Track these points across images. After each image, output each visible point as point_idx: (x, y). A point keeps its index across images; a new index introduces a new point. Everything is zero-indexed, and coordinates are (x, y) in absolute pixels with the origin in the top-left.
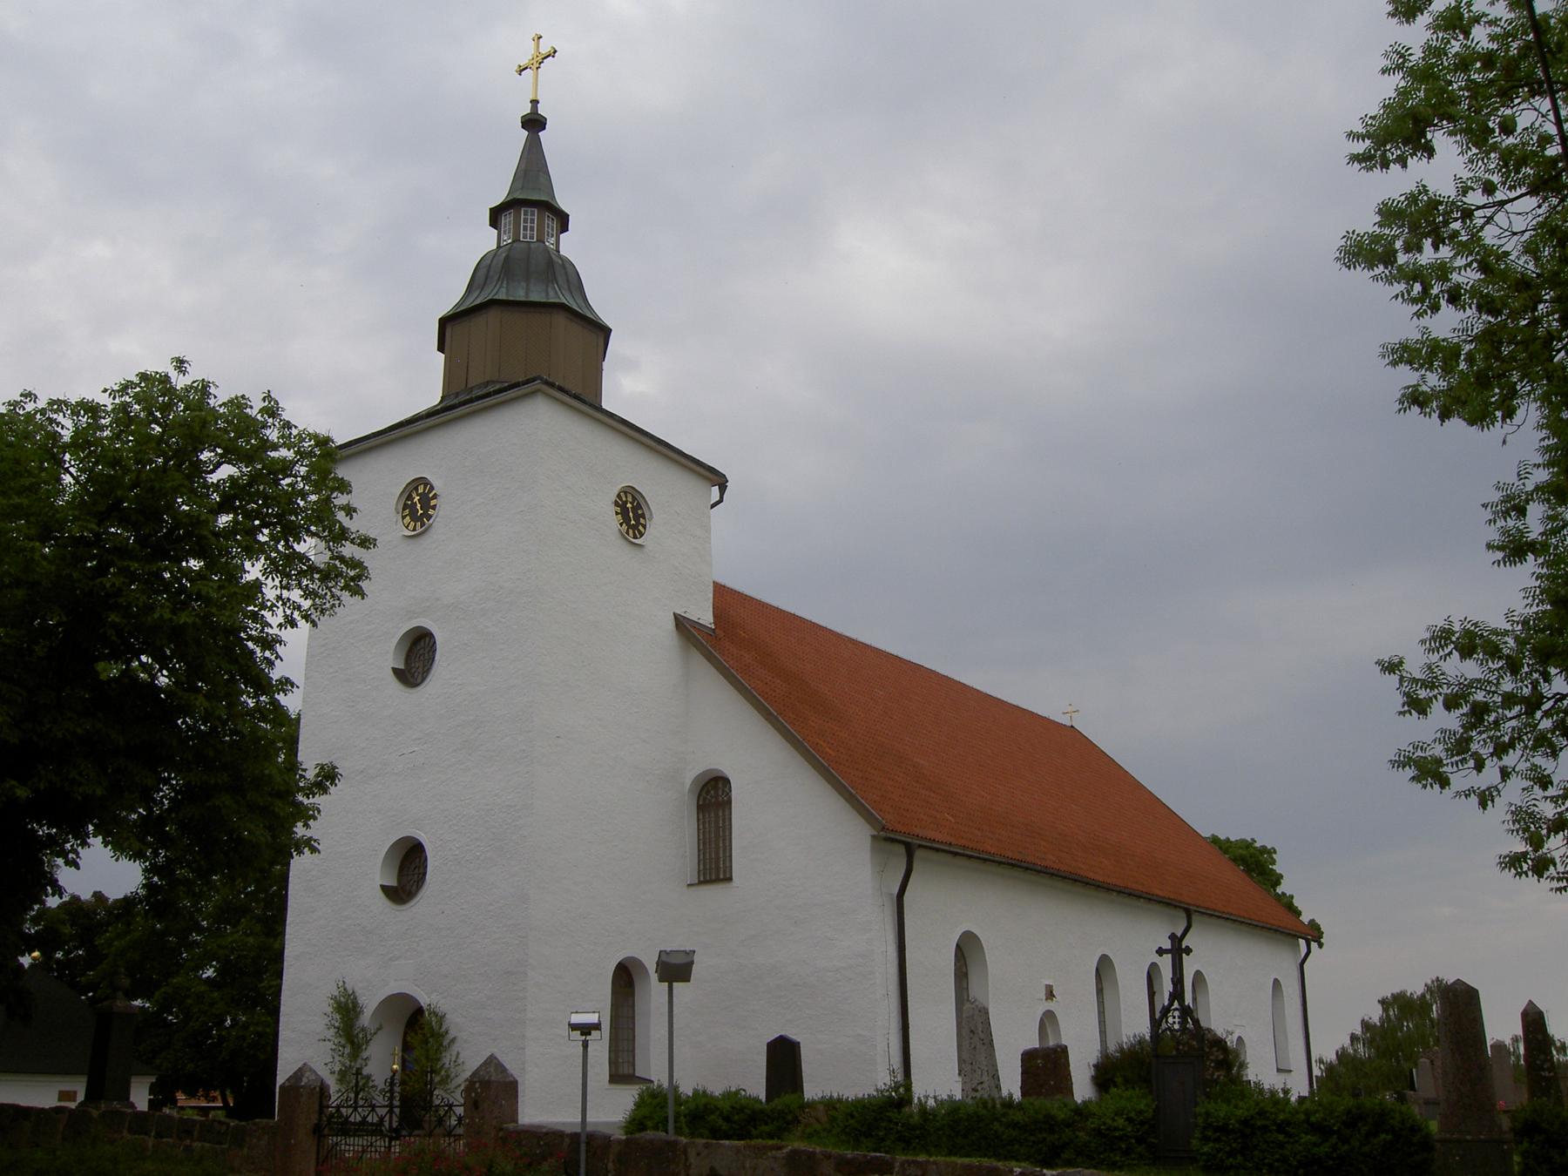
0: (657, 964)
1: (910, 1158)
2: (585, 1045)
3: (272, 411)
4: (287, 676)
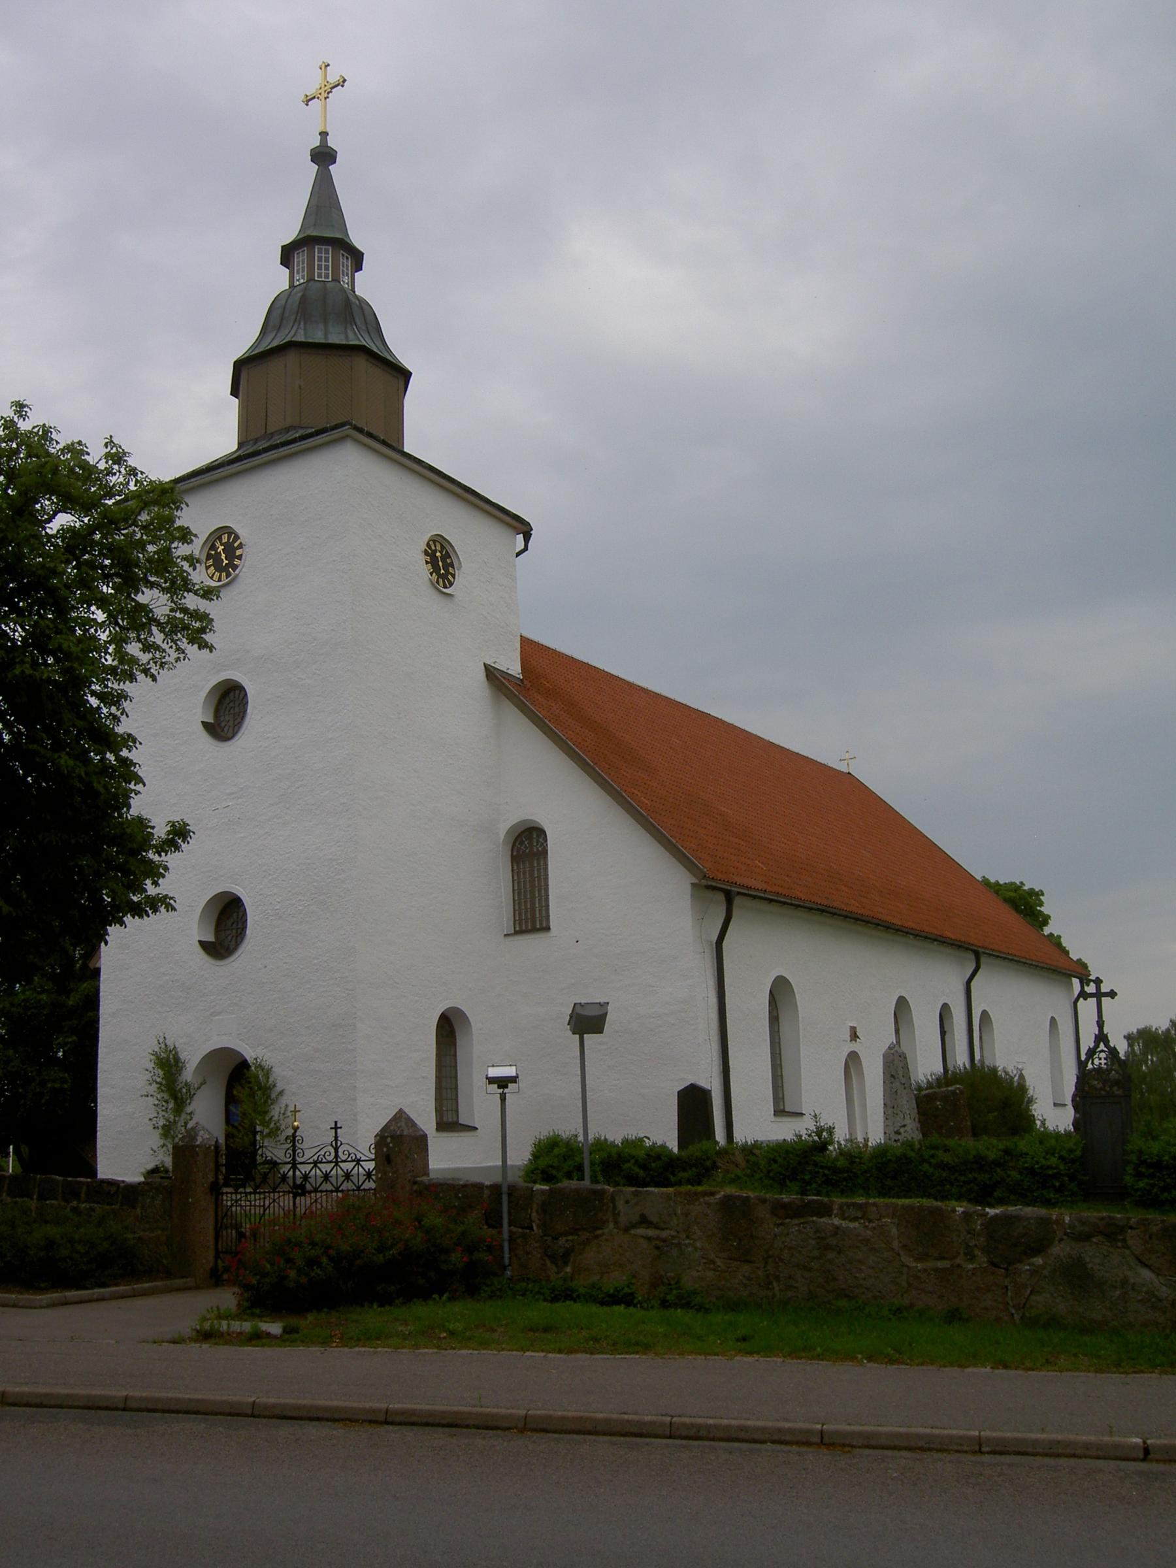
0: (571, 1017)
1: (849, 1201)
2: (503, 1098)
3: (118, 457)
4: (129, 732)
